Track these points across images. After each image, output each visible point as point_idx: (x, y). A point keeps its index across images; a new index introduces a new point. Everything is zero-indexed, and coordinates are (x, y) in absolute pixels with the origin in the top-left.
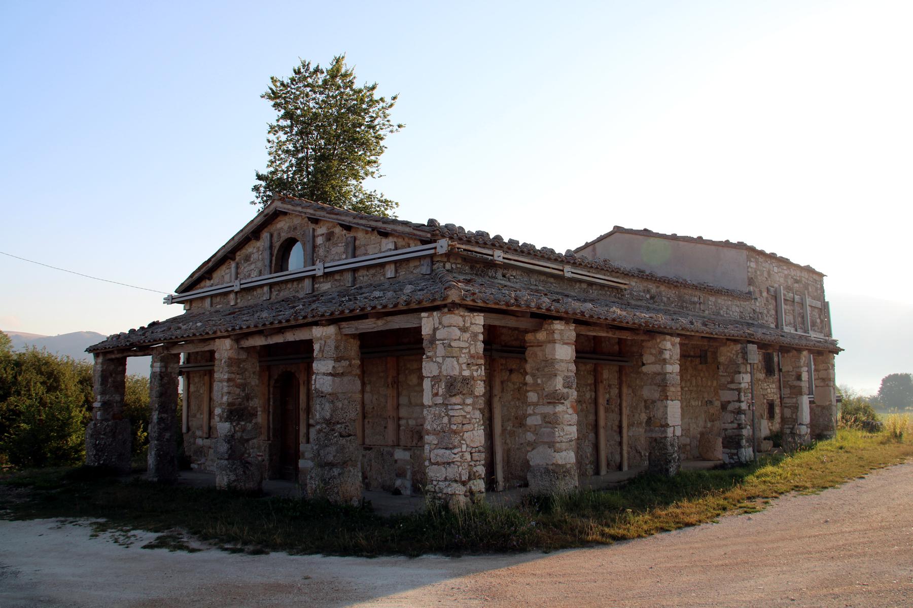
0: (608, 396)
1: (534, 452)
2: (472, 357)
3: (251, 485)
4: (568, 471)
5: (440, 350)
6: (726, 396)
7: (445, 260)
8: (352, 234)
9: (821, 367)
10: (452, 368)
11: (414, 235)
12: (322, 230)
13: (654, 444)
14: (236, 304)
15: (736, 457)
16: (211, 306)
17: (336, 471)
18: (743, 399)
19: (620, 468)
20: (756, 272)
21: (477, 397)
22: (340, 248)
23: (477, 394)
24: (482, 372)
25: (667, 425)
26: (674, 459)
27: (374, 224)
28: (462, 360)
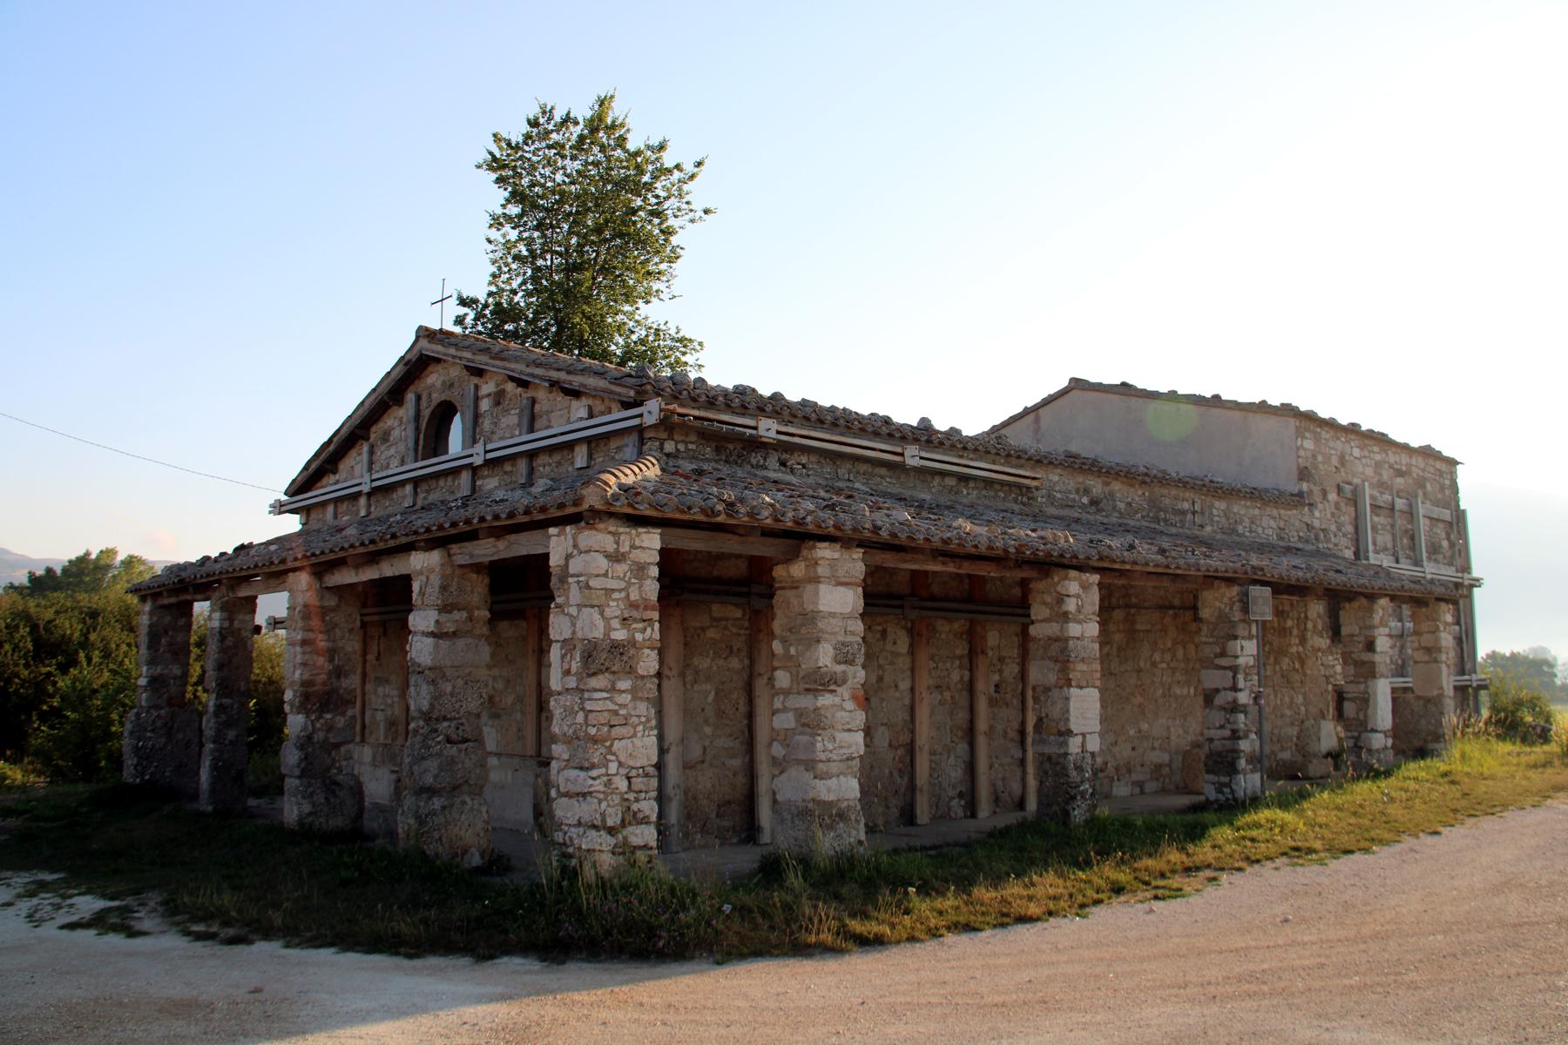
0: (996, 677)
1: (783, 777)
2: (634, 606)
3: (338, 822)
4: (842, 816)
5: (575, 595)
6: (1213, 679)
7: (665, 436)
8: (530, 394)
9: (1424, 627)
10: (592, 626)
11: (612, 392)
12: (488, 388)
13: (1047, 765)
14: (369, 513)
15: (1227, 790)
16: (335, 516)
17: (437, 803)
18: (1241, 684)
19: (1021, 804)
20: (1314, 457)
21: (643, 677)
22: (512, 419)
23: (641, 672)
24: (654, 632)
25: (1069, 733)
26: (1083, 794)
27: (555, 375)
28: (608, 612)
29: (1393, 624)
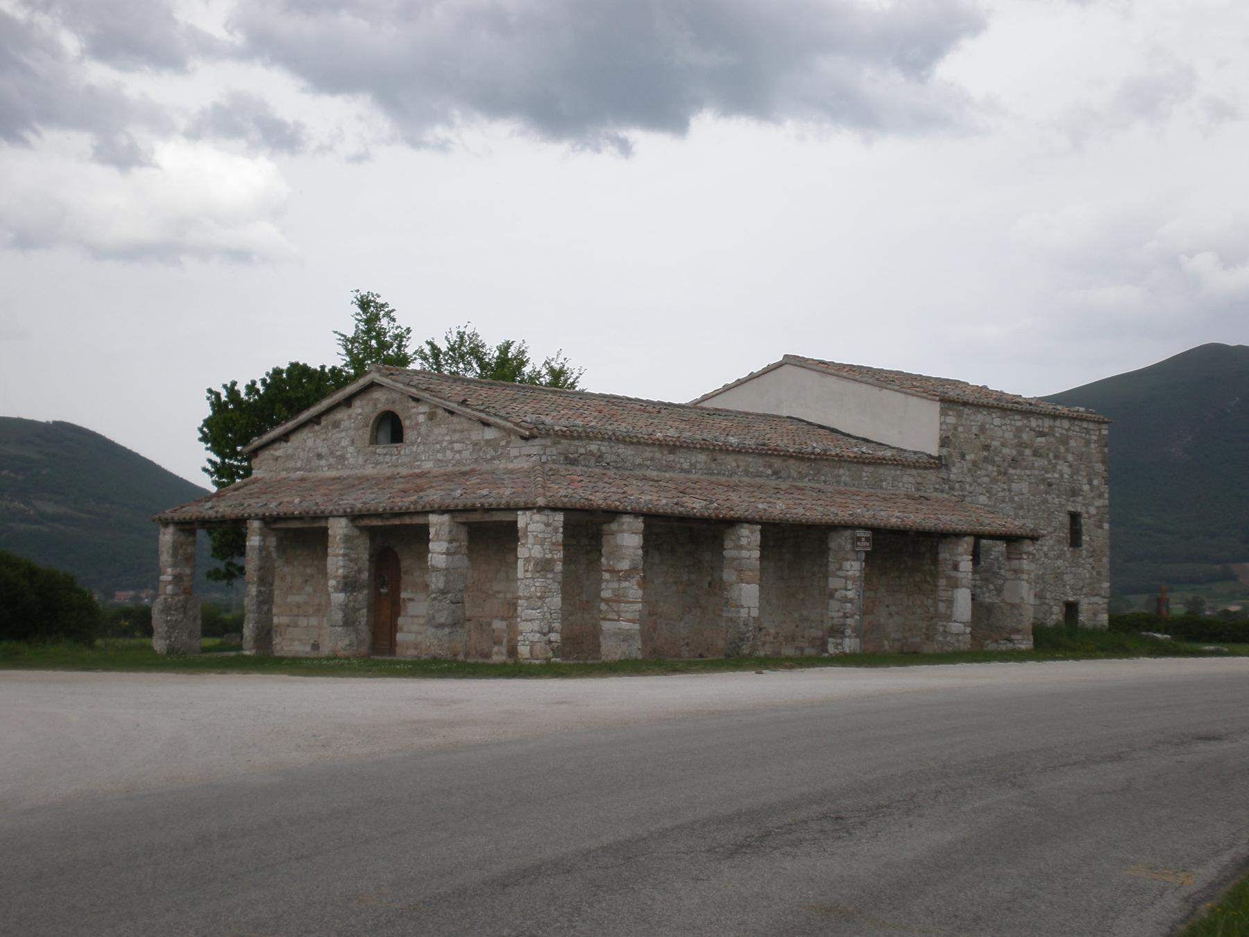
2: (554, 544)
20: (956, 429)
29: (961, 549)
